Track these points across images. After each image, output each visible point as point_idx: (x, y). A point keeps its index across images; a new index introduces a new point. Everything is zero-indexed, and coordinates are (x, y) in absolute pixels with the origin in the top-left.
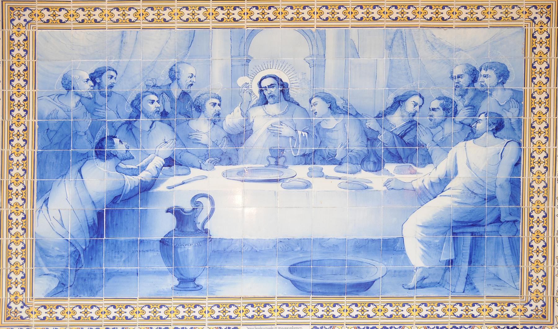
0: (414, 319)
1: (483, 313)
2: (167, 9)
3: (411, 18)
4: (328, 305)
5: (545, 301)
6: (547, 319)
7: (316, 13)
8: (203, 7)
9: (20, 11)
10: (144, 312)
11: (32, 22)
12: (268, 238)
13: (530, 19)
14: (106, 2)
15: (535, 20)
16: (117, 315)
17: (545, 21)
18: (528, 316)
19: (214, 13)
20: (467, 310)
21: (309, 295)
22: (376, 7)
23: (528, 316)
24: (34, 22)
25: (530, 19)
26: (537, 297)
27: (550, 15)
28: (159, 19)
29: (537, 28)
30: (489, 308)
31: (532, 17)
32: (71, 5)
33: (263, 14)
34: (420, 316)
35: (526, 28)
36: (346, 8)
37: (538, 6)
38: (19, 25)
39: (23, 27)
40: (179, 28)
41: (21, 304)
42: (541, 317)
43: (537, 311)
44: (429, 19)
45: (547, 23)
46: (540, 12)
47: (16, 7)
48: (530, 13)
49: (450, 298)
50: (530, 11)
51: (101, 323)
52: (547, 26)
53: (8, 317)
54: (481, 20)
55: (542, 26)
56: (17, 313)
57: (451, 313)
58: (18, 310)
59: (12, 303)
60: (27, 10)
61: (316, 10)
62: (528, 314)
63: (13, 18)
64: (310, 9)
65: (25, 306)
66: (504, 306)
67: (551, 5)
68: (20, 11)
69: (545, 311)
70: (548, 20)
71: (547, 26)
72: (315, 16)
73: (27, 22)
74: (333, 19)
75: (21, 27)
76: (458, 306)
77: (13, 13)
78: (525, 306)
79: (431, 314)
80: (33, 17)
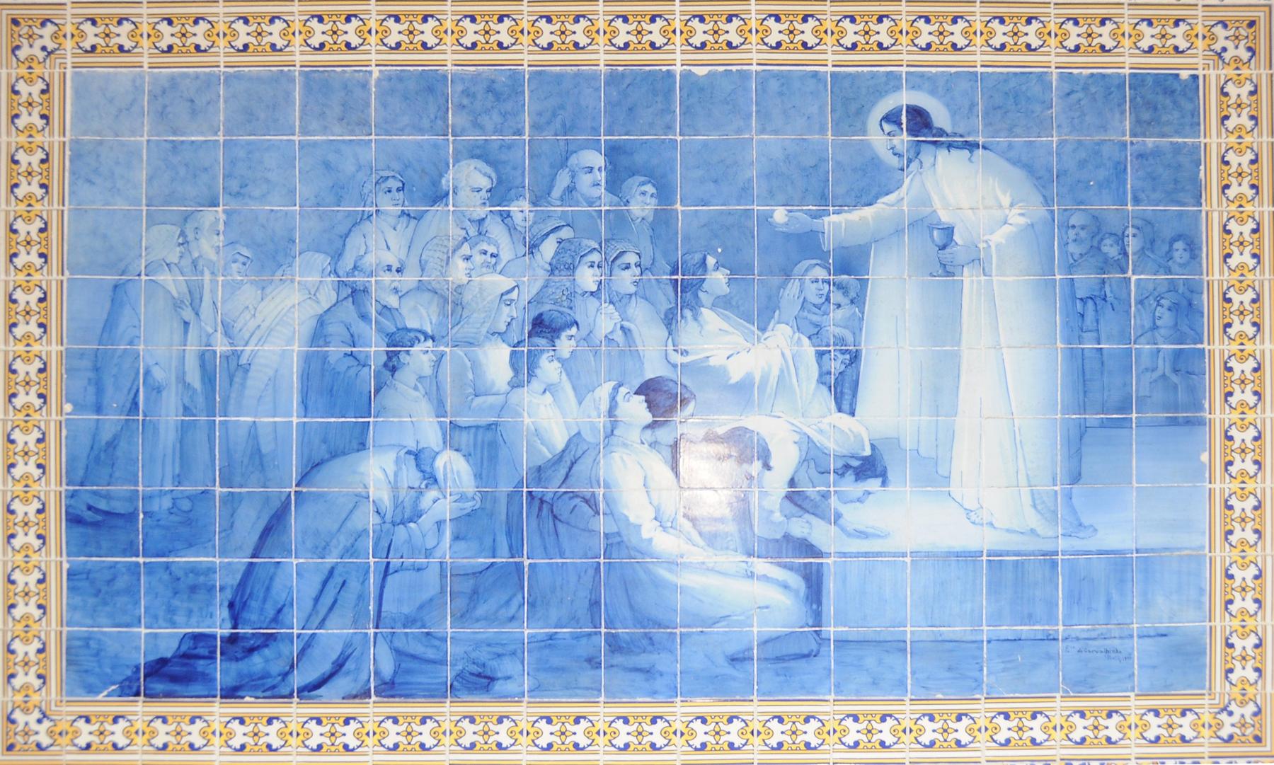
0: (1058, 747)
1: (979, 736)
3: (734, 45)
4: (1170, 712)
5: (1259, 702)
6: (1263, 743)
7: (449, 32)
8: (508, 16)
10: (357, 734)
14: (145, 5)
16: (1013, 735)
21: (593, 696)
22: (581, 19)
23: (1226, 737)
28: (563, 43)
30: (612, 729)
32: (144, 10)
33: (487, 32)
34: (919, 743)
36: (818, 20)
38: (31, 58)
40: (456, 65)
44: (699, 45)
49: (908, 702)
51: (751, 756)
54: (583, 48)
57: (986, 736)
61: (449, 25)
62: (1224, 733)
63: (17, 43)
64: (817, 23)
66: (1173, 717)
74: (335, 47)
75: (34, 65)
76: (466, 722)
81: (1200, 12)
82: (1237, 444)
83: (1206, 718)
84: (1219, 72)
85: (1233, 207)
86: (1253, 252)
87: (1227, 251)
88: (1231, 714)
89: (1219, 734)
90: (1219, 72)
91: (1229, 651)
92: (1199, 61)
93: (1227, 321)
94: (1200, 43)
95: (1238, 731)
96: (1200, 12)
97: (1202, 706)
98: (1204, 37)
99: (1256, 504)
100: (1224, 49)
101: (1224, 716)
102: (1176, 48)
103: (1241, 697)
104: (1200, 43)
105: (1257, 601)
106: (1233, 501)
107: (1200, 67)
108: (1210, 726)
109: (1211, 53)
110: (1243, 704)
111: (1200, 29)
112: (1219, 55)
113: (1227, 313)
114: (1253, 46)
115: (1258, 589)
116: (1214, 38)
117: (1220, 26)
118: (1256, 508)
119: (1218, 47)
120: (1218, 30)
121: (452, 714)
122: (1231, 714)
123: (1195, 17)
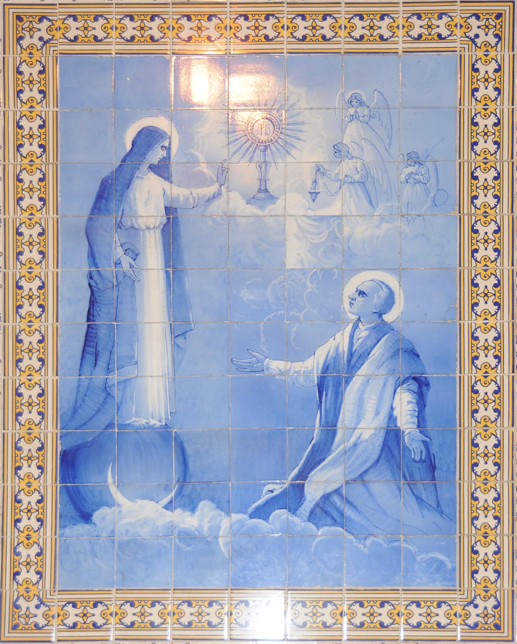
2: (386, 17)
9: (33, 23)
11: (52, 42)
13: (468, 37)
15: (476, 40)
17: (493, 41)
18: (472, 625)
19: (348, 25)
20: (429, 615)
25: (468, 37)
27: (501, 32)
29: (480, 54)
31: (472, 34)
35: (463, 53)
37: (481, 15)
39: (38, 50)
41: (36, 602)
42: (24, 17)
45: (496, 45)
46: (485, 25)
47: (26, 16)
48: (468, 28)
50: (469, 24)
52: (496, 50)
55: (487, 51)
58: (32, 612)
59: (21, 598)
60: (45, 20)
65: (42, 605)
67: (17, 16)
68: (33, 23)
70: (497, 40)
71: (496, 50)
72: (343, 33)
73: (44, 42)
77: (21, 26)
79: (369, 621)
82: (36, 195)
85: (26, 108)
86: (21, 345)
87: (42, 238)
93: (43, 184)
95: (35, 25)
99: (21, 202)
100: (477, 36)
105: (20, 73)
106: (39, 204)
110: (31, 46)
112: (473, 41)
113: (43, 190)
115: (20, 82)
118: (21, 199)
121: (117, 599)
122: (41, 39)
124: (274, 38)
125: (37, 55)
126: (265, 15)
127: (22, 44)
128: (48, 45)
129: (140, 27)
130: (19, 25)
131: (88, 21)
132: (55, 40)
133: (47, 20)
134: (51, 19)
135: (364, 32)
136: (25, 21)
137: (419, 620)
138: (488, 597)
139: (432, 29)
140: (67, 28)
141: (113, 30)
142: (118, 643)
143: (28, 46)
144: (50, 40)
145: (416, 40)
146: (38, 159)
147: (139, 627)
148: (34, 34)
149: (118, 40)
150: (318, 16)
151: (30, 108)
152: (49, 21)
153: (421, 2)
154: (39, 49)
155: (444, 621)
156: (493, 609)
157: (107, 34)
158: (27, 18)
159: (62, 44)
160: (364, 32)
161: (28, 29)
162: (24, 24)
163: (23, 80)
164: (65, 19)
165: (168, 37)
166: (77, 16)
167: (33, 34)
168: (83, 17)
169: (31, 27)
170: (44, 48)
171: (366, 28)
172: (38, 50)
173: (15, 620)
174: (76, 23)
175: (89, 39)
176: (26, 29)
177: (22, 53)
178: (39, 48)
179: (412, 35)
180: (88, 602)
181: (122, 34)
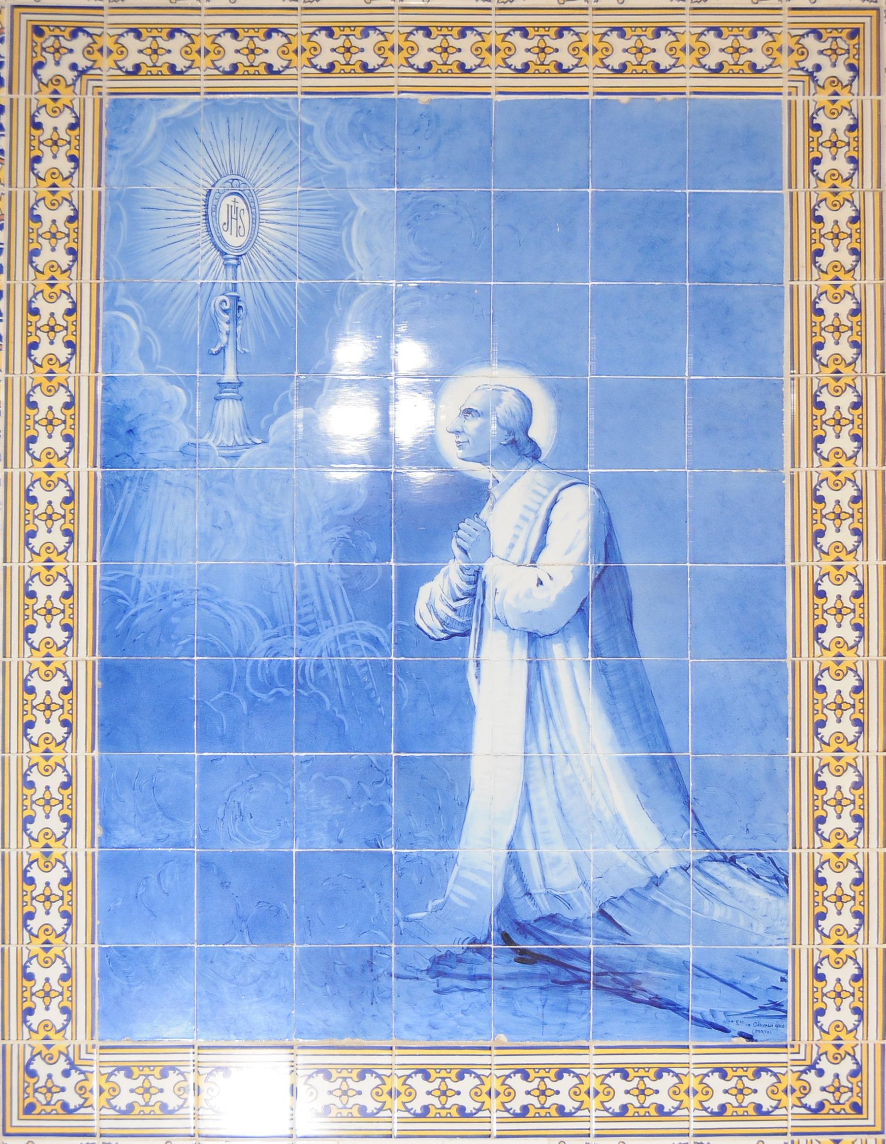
9: (833, 1102)
12: (667, 731)
24: (98, 72)
26: (838, 1046)
39: (826, 1053)
42: (849, 1111)
43: (838, 1089)
53: (69, 693)
56: (841, 1086)
69: (858, 1090)
78: (804, 1076)
80: (96, 56)
81: (785, 18)
83: (106, 62)
84: (72, 1043)
88: (74, 67)
89: (90, 40)
90: (72, 1043)
91: (35, 132)
92: (783, 83)
94: (785, 60)
95: (830, 1097)
96: (785, 18)
97: (113, 78)
98: (791, 51)
101: (82, 63)
102: (753, 66)
103: (835, 1050)
104: (785, 60)
107: (785, 90)
108: (101, 50)
109: (84, 1068)
111: (785, 41)
114: (855, 62)
116: (804, 52)
117: (72, 1107)
119: (809, 65)
120: (810, 42)
122: (74, 67)
123: (777, 24)
124: (612, 1075)
125: (827, 1044)
126: (527, 1116)
127: (854, 1063)
128: (808, 1062)
129: (546, 1096)
130: (858, 1096)
131: (737, 1104)
132: (796, 1072)
133: (810, 1106)
134: (803, 1109)
135: (456, 1086)
136: (848, 1103)
137: (172, 41)
138: (52, 83)
139: (151, 1095)
140: (674, 1092)
141: (693, 1089)
142: (98, 2)
143: (842, 1059)
144: (804, 1072)
145: (764, 1067)
146: (827, 858)
147: (256, 30)
148: (831, 1081)
149: (585, 1072)
150: (436, 1113)
151: (841, 949)
152: (806, 1104)
153: (455, 1137)
154: (824, 1055)
155: (226, 40)
156: (44, 61)
157: (506, 1083)
158: (844, 1110)
159: (783, 1064)
160: (456, 1086)
161: (49, 1095)
162: (849, 1098)
163: (851, 998)
164: (678, 1108)
165: (498, 1078)
166: (557, 1115)
167: (57, 1087)
168: (547, 1113)
169: (837, 1094)
170: (815, 1056)
171: (453, 1093)
172: (826, 1053)
173: (854, 45)
174: (460, 1104)
175: (438, 1075)
176: (846, 1090)
177: (853, 1048)
178: (823, 1057)
179: (375, 1078)
180: (246, 73)
181: (479, 1083)
